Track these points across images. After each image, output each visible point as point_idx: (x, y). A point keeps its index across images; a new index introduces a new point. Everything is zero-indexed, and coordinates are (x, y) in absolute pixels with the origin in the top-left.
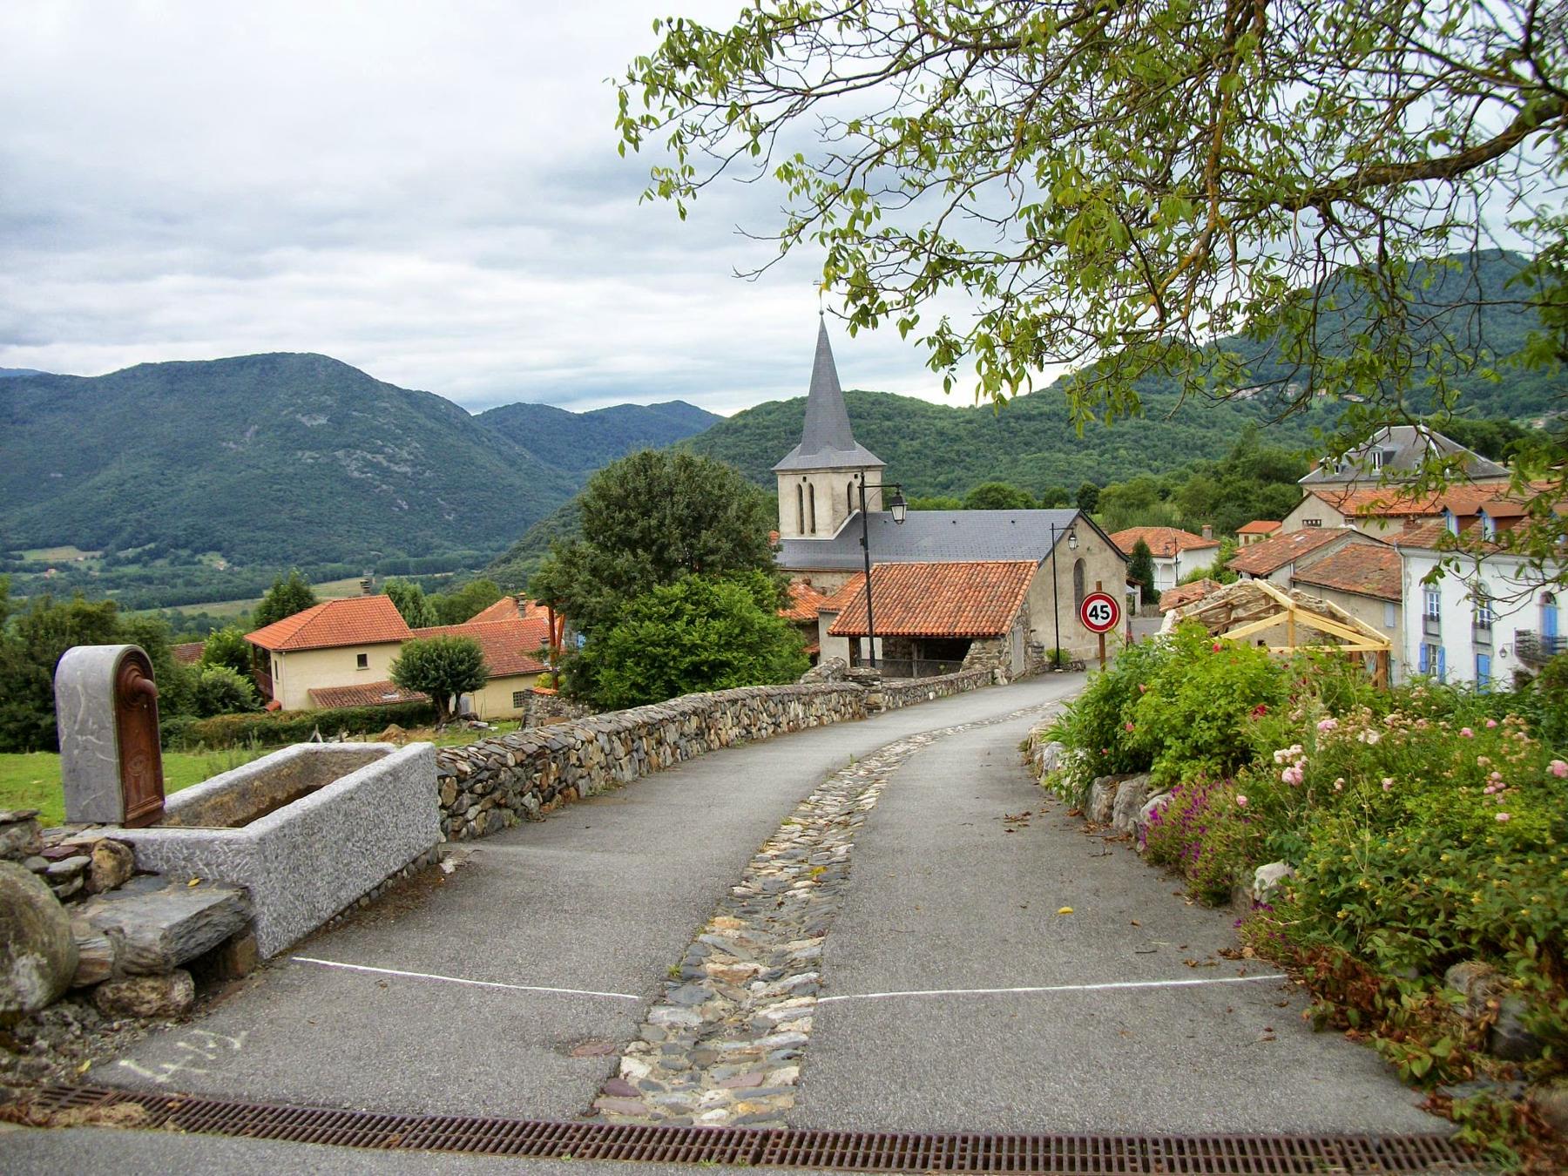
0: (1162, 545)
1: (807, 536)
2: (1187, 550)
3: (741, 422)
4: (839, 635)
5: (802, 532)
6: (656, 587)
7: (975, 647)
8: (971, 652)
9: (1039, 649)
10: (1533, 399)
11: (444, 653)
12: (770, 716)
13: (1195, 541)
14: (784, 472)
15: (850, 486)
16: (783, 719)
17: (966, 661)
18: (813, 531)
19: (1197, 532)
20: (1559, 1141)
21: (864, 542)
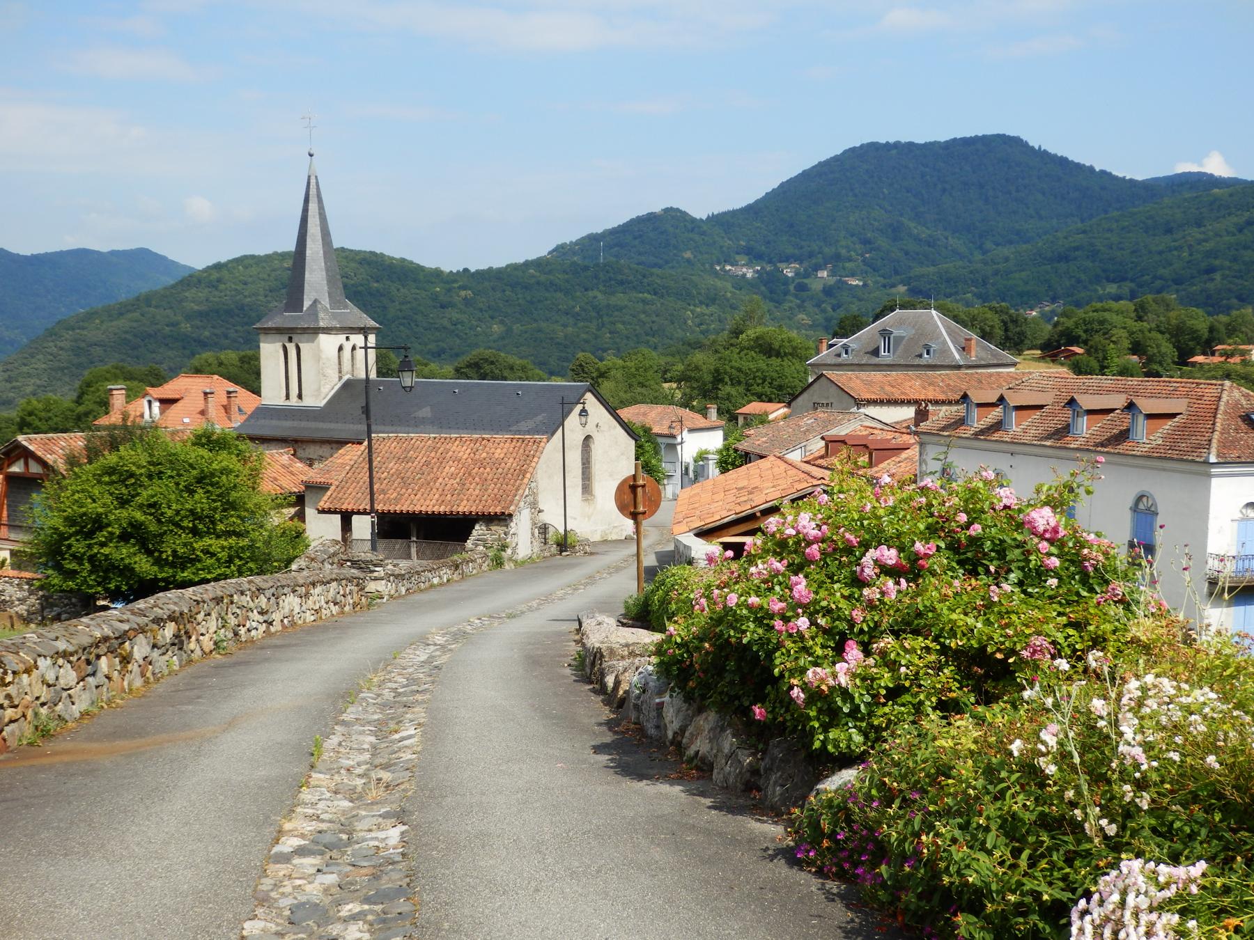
0: (666, 423)
1: (294, 401)
2: (691, 430)
3: (215, 275)
4: (329, 512)
5: (288, 397)
6: (950, 594)
7: (479, 530)
8: (474, 533)
9: (544, 529)
10: (963, 316)
11: (1224, 632)
12: (261, 613)
13: (699, 421)
14: (267, 331)
15: (341, 349)
16: (277, 617)
17: (469, 544)
18: (300, 396)
19: (704, 412)
20: (1215, 913)
21: (366, 410)
